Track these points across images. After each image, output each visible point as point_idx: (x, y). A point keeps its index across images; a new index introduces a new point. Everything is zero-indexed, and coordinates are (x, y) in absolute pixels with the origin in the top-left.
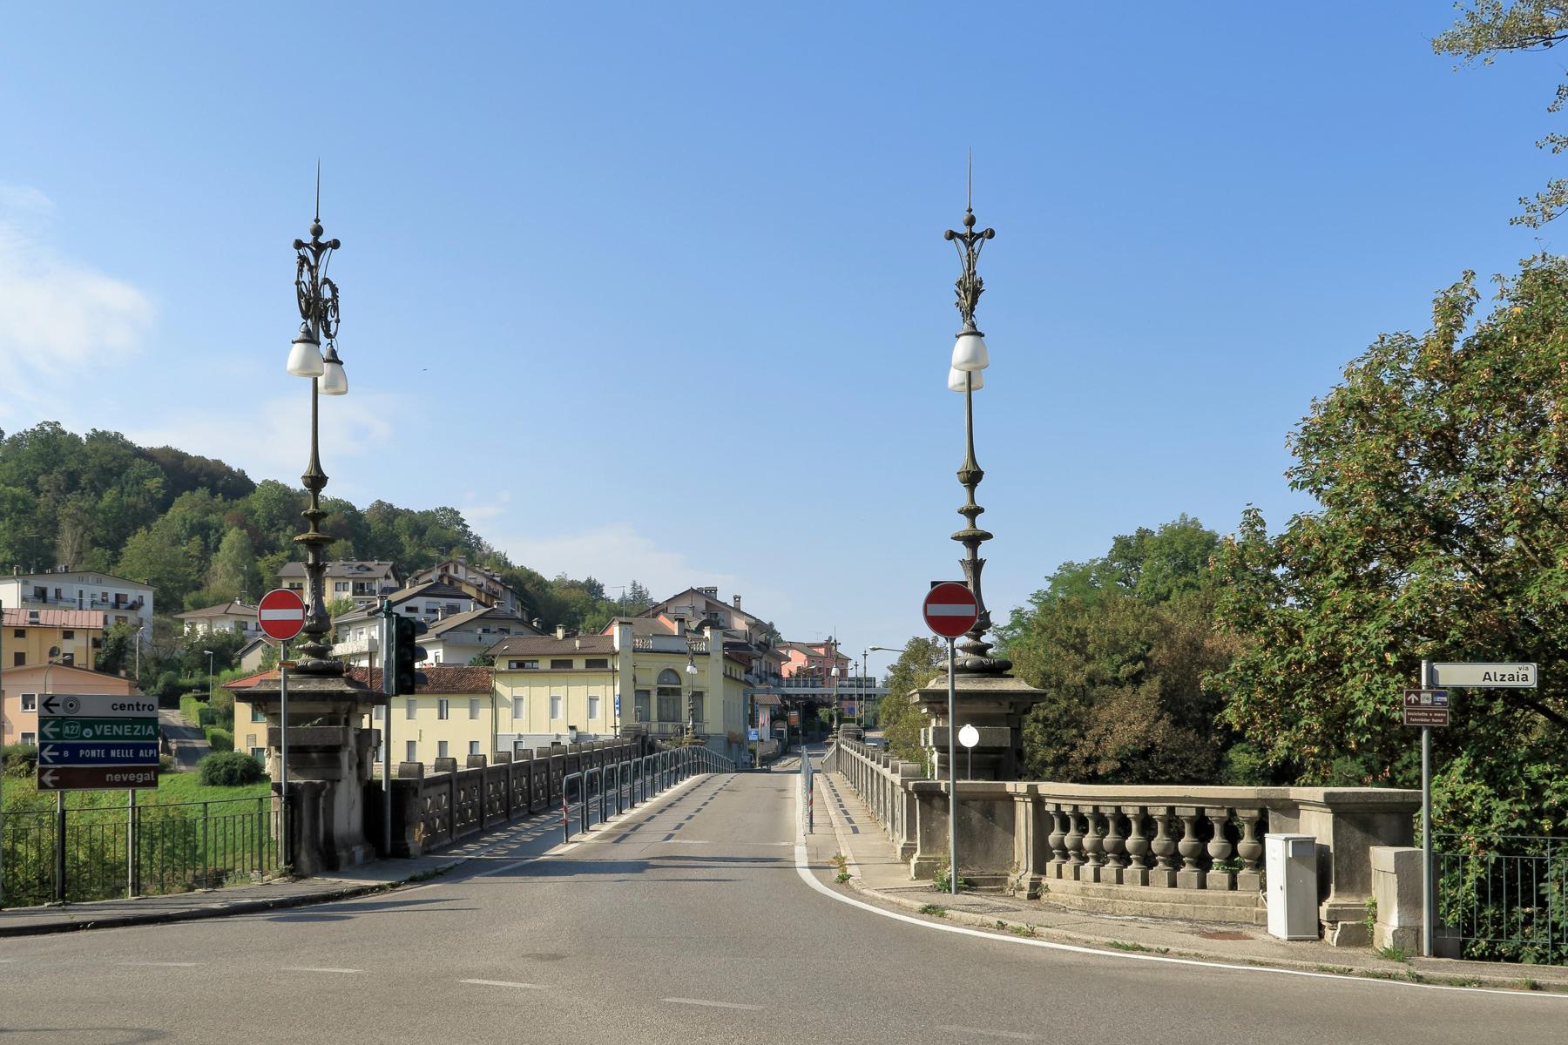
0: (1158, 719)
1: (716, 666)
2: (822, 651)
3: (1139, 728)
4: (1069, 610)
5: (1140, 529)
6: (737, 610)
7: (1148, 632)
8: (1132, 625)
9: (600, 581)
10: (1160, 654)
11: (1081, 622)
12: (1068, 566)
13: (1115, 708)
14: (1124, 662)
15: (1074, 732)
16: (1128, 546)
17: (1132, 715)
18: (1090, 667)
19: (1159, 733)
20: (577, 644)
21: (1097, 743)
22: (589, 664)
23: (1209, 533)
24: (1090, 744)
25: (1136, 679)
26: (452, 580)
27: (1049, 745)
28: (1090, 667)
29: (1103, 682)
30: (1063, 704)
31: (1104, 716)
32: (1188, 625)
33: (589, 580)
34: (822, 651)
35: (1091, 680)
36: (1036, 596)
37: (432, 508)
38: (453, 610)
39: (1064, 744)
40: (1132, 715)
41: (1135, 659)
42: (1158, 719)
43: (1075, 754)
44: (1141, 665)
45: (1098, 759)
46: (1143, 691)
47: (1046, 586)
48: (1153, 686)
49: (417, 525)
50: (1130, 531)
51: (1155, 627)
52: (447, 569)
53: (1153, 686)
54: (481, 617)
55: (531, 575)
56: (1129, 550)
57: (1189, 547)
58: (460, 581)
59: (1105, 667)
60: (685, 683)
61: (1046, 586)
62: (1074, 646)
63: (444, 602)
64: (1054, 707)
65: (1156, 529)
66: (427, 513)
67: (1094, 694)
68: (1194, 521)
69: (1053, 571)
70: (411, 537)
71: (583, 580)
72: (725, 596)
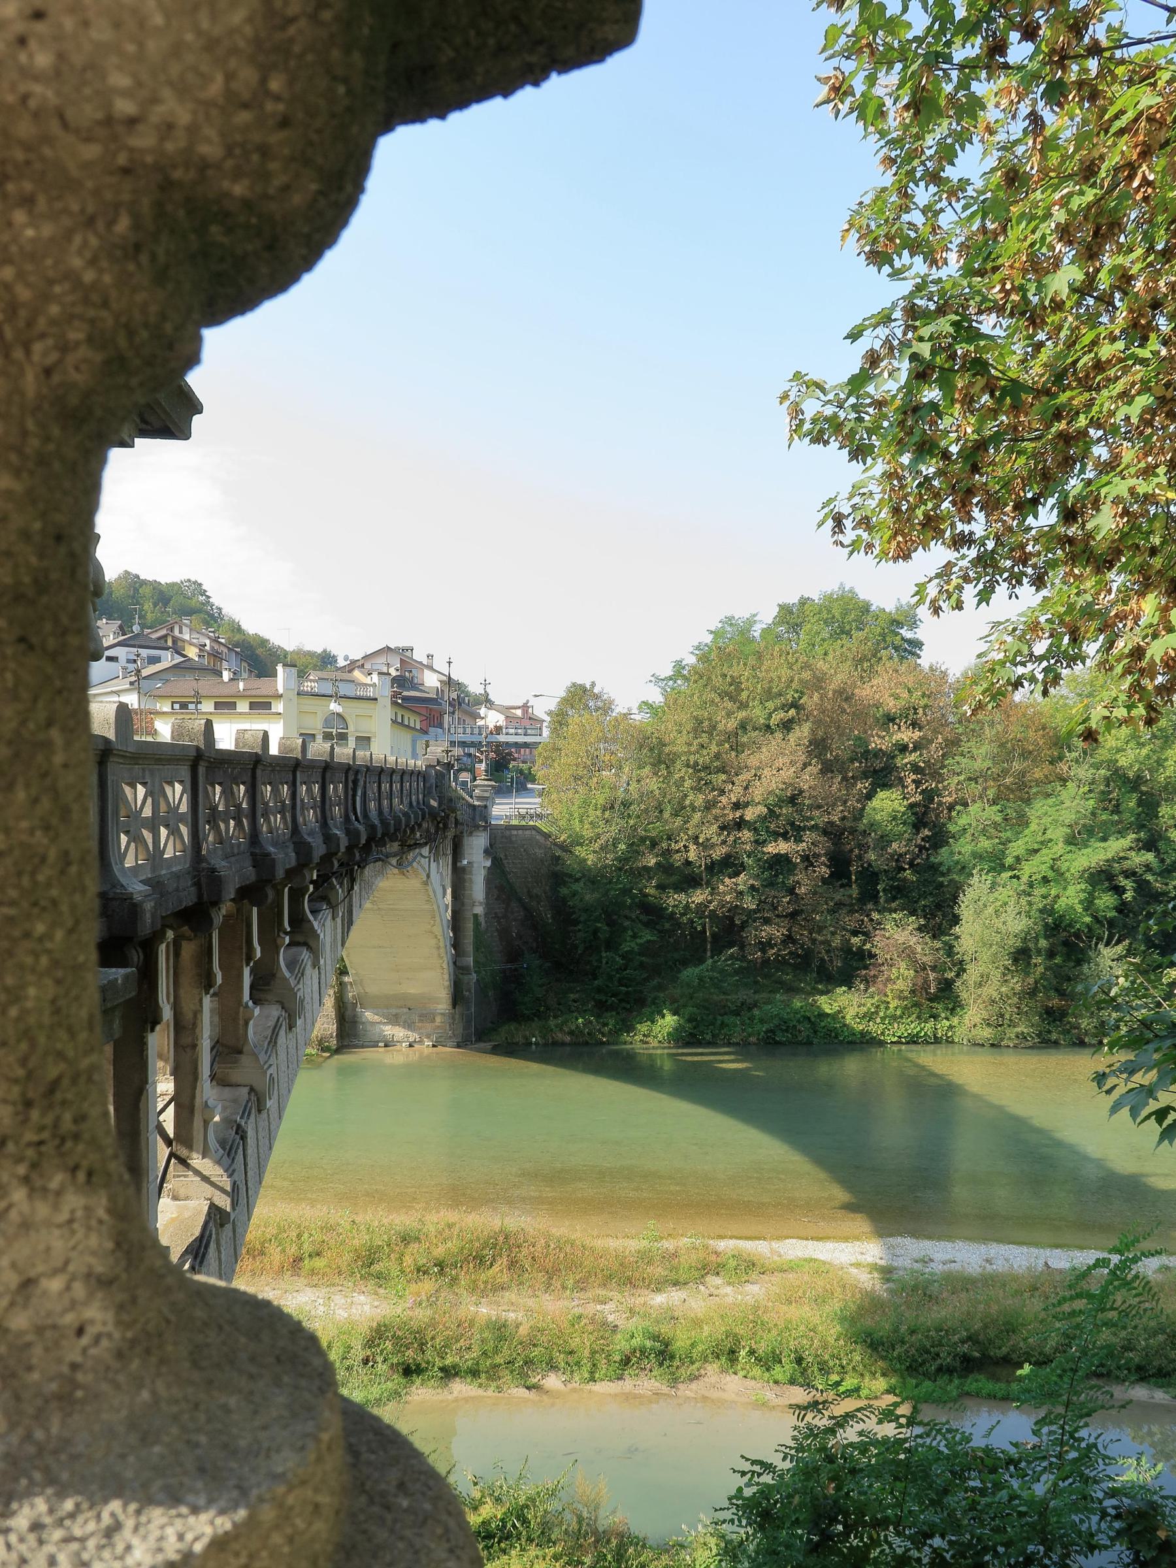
0: (805, 765)
1: (384, 713)
2: (519, 712)
3: (788, 774)
4: (725, 656)
5: (802, 597)
6: (487, 701)
7: (801, 681)
8: (785, 673)
9: (334, 652)
10: (811, 701)
11: (735, 671)
12: (729, 621)
13: (764, 754)
14: (775, 710)
15: (724, 777)
16: (791, 613)
17: (781, 761)
18: (742, 714)
19: (808, 780)
20: (241, 685)
21: (746, 788)
22: (253, 706)
23: (864, 601)
24: (738, 789)
25: (787, 726)
26: (175, 640)
27: (700, 790)
28: (742, 714)
29: (755, 729)
30: (714, 748)
31: (753, 761)
32: (839, 677)
33: (325, 651)
34: (519, 712)
35: (743, 726)
36: (698, 648)
37: (177, 579)
38: (154, 660)
39: (713, 790)
40: (781, 761)
41: (785, 707)
42: (805, 765)
43: (724, 799)
44: (792, 712)
45: (747, 805)
46: (792, 737)
47: (708, 639)
48: (803, 732)
49: (161, 593)
50: (793, 599)
51: (806, 675)
52: (172, 629)
53: (803, 732)
54: (175, 666)
55: (264, 642)
56: (792, 617)
57: (845, 614)
58: (184, 641)
59: (758, 713)
60: (351, 728)
61: (708, 639)
62: (727, 694)
63: (144, 653)
64: (705, 752)
65: (816, 597)
66: (174, 584)
67: (745, 739)
68: (851, 591)
69: (715, 625)
70: (155, 605)
71: (319, 651)
72: (419, 656)
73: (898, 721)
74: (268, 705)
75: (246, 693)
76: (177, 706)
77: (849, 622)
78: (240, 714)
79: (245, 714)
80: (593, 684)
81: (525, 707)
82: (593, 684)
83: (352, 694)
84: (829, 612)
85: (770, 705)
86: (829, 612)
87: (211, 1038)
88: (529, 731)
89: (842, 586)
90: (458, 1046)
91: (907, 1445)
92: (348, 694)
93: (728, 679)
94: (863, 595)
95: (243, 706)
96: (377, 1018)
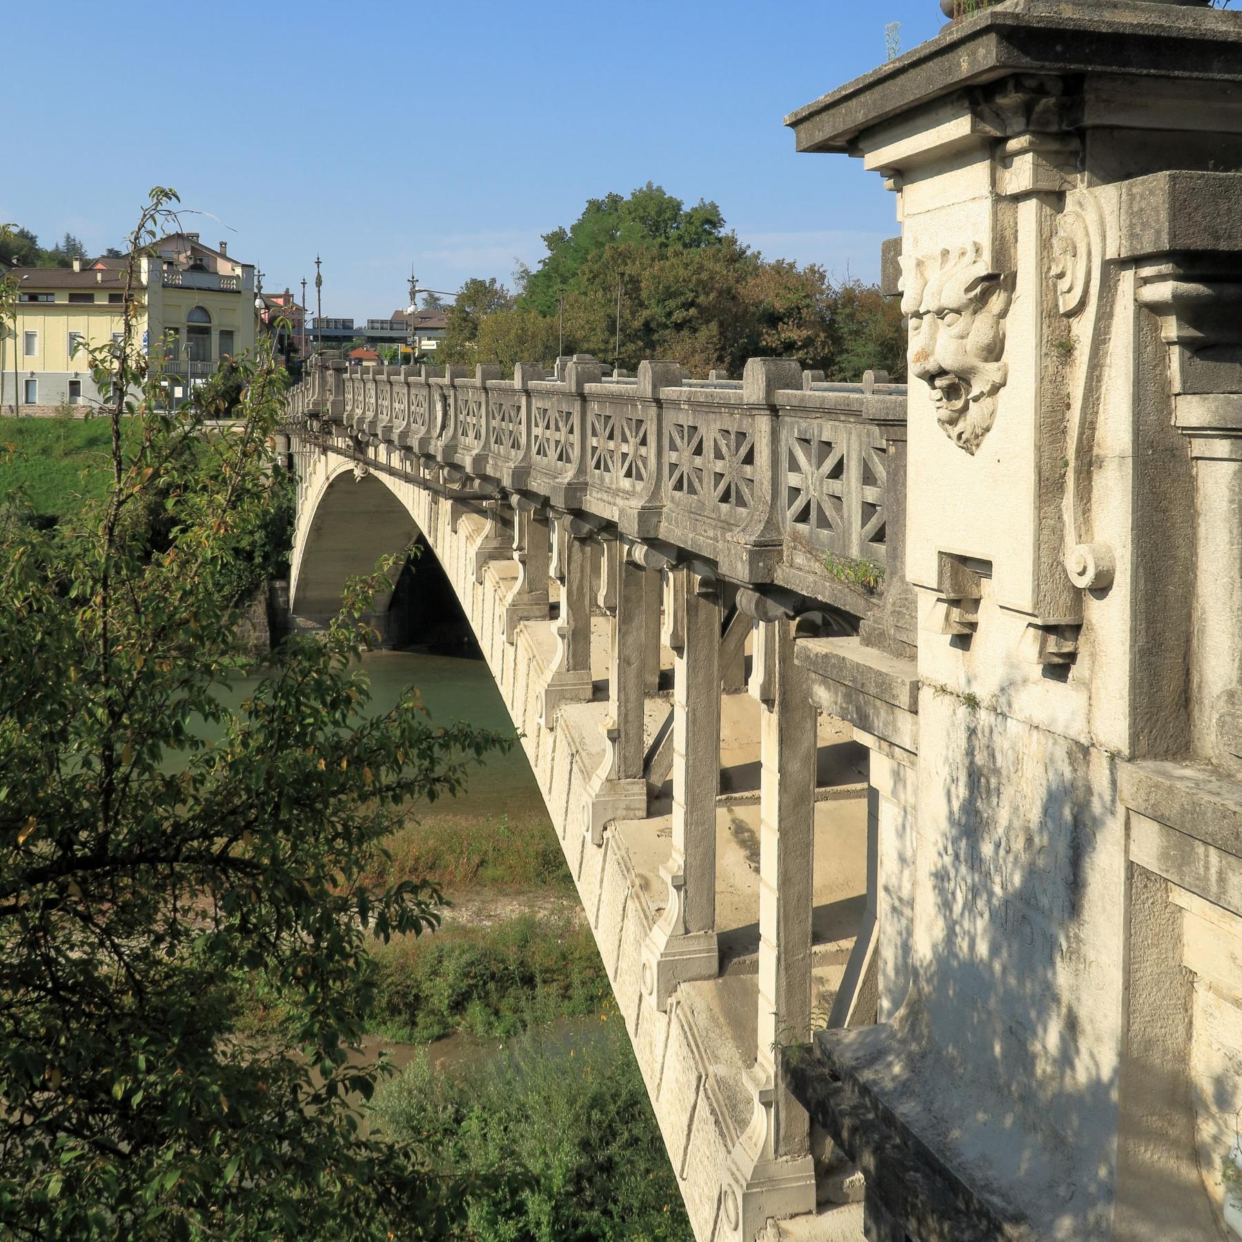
2: (280, 301)
22: (73, 297)
50: (601, 196)
65: (627, 197)
73: (786, 320)
74: (90, 298)
75: (106, 285)
76: (26, 298)
77: (664, 221)
78: (100, 306)
79: (66, 306)
80: (493, 281)
81: (287, 296)
82: (493, 281)
83: (216, 287)
84: (645, 208)
85: (672, 303)
86: (645, 208)
87: (754, 968)
88: (395, 326)
89: (649, 185)
90: (394, 649)
91: (194, 663)
92: (212, 287)
93: (626, 278)
94: (671, 192)
95: (101, 300)
96: (310, 624)
